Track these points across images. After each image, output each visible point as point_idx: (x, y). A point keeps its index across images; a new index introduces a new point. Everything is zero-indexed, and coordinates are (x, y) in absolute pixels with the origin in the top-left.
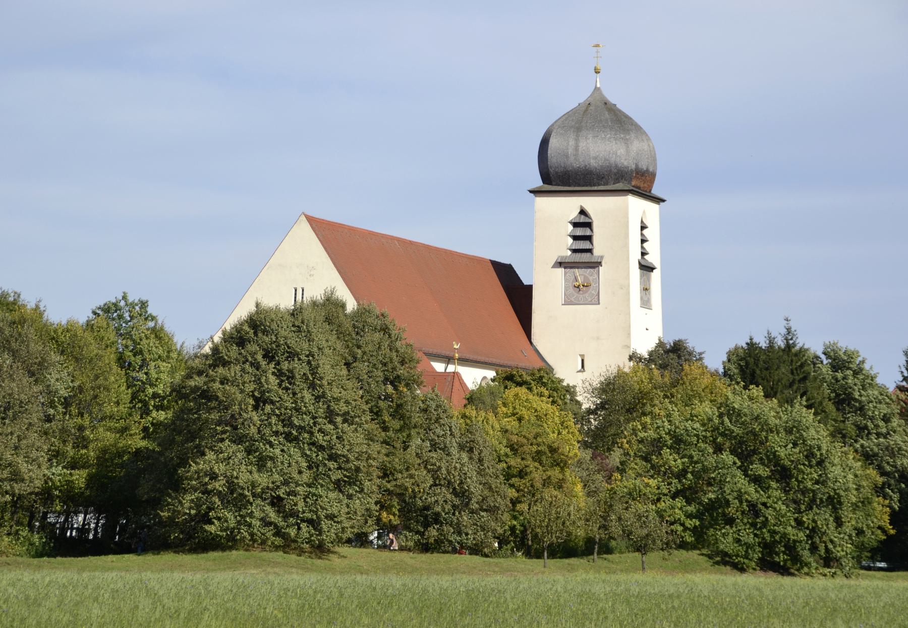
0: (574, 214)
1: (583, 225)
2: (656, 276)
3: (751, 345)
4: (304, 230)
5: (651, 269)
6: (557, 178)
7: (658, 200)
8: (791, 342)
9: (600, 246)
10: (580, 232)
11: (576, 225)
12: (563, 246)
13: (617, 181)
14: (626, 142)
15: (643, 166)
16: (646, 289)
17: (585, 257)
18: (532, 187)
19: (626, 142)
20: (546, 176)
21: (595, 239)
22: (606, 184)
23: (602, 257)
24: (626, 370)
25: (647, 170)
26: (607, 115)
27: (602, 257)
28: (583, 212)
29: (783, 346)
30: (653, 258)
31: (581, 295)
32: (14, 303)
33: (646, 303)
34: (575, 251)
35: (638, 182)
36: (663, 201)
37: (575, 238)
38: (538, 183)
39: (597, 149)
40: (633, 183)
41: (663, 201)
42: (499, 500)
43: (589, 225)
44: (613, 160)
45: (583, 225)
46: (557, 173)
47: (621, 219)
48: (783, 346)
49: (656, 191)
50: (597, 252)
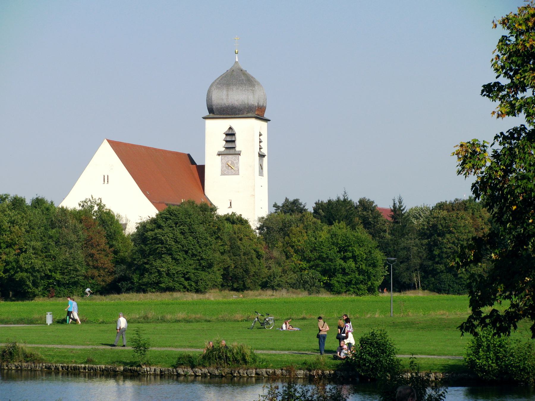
0: (226, 129)
1: (230, 135)
2: (265, 159)
3: (373, 202)
4: (106, 141)
5: (264, 156)
6: (216, 112)
7: (267, 120)
8: (346, 197)
9: (239, 146)
10: (229, 138)
11: (227, 135)
12: (221, 146)
13: (248, 112)
14: (253, 92)
15: (261, 104)
16: (261, 166)
17: (232, 151)
18: (204, 116)
19: (253, 92)
20: (211, 110)
21: (237, 142)
22: (242, 114)
23: (241, 151)
24: (309, 210)
25: (263, 106)
26: (243, 77)
27: (241, 151)
28: (230, 128)
29: (342, 200)
30: (265, 151)
31: (230, 169)
32: (345, 200)
33: (261, 174)
34: (226, 148)
35: (258, 113)
36: (269, 120)
37: (227, 141)
38: (207, 113)
39: (237, 97)
40: (256, 113)
41: (269, 120)
42: (462, 243)
43: (234, 135)
44: (246, 102)
45: (230, 135)
46: (217, 108)
47: (247, 129)
48: (342, 200)
49: (266, 116)
50: (238, 149)
